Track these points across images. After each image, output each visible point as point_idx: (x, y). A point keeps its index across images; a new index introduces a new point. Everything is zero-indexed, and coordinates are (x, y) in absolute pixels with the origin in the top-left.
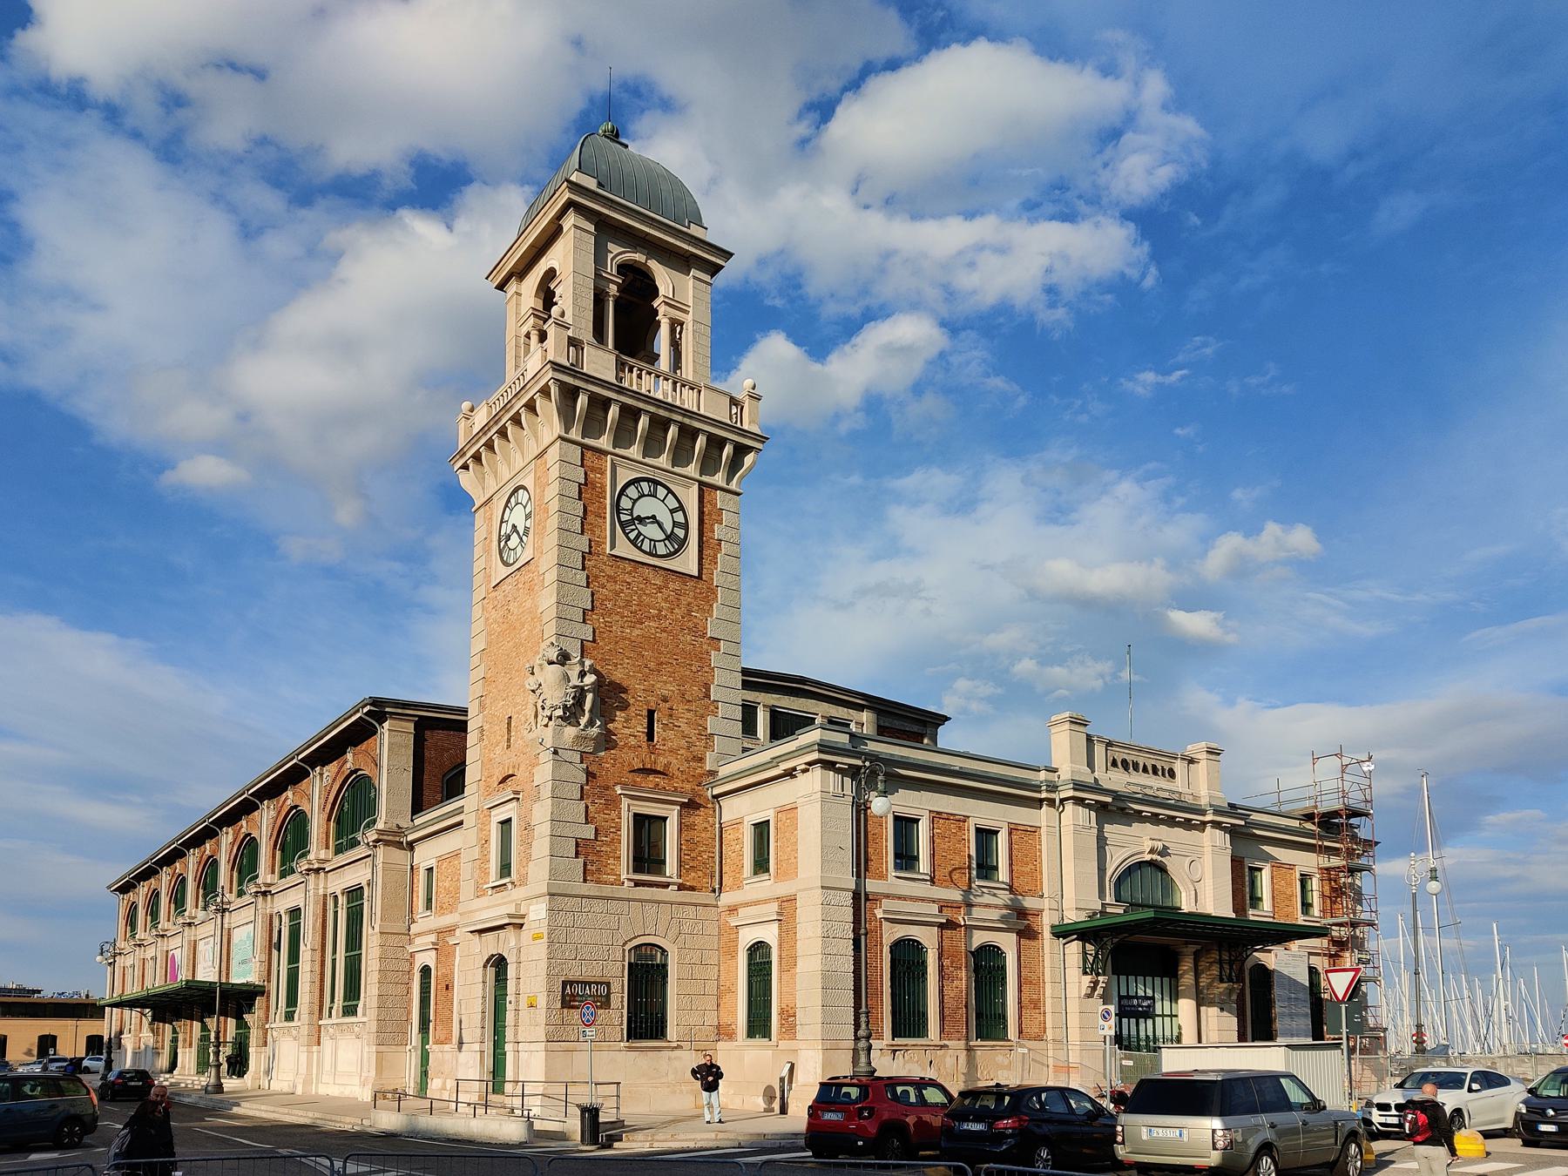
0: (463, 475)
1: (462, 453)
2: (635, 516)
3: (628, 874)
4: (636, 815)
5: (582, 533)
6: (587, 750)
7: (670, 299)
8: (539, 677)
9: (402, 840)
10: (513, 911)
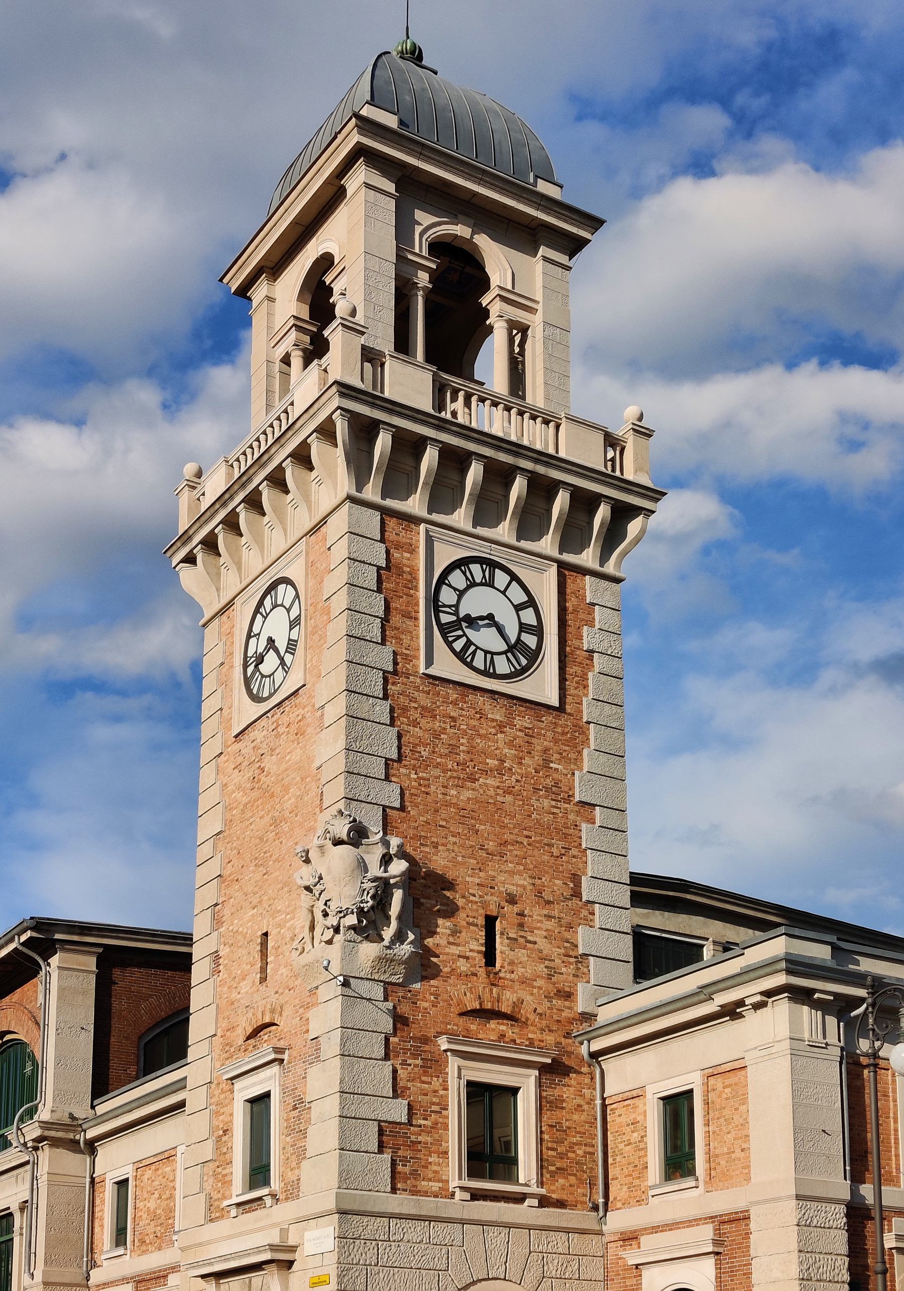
0: (186, 574)
1: (186, 538)
2: (461, 616)
3: (460, 1178)
4: (470, 1084)
5: (383, 643)
6: (394, 979)
7: (508, 291)
8: (319, 865)
9: (77, 1137)
10: (276, 1241)
